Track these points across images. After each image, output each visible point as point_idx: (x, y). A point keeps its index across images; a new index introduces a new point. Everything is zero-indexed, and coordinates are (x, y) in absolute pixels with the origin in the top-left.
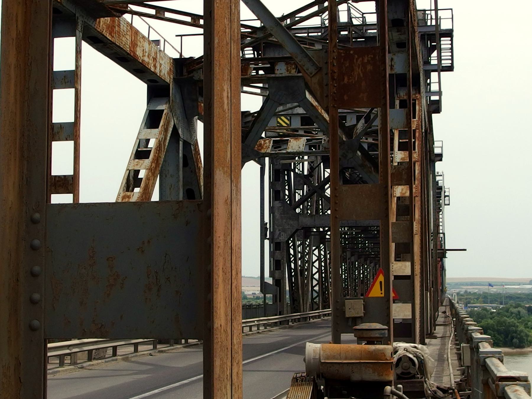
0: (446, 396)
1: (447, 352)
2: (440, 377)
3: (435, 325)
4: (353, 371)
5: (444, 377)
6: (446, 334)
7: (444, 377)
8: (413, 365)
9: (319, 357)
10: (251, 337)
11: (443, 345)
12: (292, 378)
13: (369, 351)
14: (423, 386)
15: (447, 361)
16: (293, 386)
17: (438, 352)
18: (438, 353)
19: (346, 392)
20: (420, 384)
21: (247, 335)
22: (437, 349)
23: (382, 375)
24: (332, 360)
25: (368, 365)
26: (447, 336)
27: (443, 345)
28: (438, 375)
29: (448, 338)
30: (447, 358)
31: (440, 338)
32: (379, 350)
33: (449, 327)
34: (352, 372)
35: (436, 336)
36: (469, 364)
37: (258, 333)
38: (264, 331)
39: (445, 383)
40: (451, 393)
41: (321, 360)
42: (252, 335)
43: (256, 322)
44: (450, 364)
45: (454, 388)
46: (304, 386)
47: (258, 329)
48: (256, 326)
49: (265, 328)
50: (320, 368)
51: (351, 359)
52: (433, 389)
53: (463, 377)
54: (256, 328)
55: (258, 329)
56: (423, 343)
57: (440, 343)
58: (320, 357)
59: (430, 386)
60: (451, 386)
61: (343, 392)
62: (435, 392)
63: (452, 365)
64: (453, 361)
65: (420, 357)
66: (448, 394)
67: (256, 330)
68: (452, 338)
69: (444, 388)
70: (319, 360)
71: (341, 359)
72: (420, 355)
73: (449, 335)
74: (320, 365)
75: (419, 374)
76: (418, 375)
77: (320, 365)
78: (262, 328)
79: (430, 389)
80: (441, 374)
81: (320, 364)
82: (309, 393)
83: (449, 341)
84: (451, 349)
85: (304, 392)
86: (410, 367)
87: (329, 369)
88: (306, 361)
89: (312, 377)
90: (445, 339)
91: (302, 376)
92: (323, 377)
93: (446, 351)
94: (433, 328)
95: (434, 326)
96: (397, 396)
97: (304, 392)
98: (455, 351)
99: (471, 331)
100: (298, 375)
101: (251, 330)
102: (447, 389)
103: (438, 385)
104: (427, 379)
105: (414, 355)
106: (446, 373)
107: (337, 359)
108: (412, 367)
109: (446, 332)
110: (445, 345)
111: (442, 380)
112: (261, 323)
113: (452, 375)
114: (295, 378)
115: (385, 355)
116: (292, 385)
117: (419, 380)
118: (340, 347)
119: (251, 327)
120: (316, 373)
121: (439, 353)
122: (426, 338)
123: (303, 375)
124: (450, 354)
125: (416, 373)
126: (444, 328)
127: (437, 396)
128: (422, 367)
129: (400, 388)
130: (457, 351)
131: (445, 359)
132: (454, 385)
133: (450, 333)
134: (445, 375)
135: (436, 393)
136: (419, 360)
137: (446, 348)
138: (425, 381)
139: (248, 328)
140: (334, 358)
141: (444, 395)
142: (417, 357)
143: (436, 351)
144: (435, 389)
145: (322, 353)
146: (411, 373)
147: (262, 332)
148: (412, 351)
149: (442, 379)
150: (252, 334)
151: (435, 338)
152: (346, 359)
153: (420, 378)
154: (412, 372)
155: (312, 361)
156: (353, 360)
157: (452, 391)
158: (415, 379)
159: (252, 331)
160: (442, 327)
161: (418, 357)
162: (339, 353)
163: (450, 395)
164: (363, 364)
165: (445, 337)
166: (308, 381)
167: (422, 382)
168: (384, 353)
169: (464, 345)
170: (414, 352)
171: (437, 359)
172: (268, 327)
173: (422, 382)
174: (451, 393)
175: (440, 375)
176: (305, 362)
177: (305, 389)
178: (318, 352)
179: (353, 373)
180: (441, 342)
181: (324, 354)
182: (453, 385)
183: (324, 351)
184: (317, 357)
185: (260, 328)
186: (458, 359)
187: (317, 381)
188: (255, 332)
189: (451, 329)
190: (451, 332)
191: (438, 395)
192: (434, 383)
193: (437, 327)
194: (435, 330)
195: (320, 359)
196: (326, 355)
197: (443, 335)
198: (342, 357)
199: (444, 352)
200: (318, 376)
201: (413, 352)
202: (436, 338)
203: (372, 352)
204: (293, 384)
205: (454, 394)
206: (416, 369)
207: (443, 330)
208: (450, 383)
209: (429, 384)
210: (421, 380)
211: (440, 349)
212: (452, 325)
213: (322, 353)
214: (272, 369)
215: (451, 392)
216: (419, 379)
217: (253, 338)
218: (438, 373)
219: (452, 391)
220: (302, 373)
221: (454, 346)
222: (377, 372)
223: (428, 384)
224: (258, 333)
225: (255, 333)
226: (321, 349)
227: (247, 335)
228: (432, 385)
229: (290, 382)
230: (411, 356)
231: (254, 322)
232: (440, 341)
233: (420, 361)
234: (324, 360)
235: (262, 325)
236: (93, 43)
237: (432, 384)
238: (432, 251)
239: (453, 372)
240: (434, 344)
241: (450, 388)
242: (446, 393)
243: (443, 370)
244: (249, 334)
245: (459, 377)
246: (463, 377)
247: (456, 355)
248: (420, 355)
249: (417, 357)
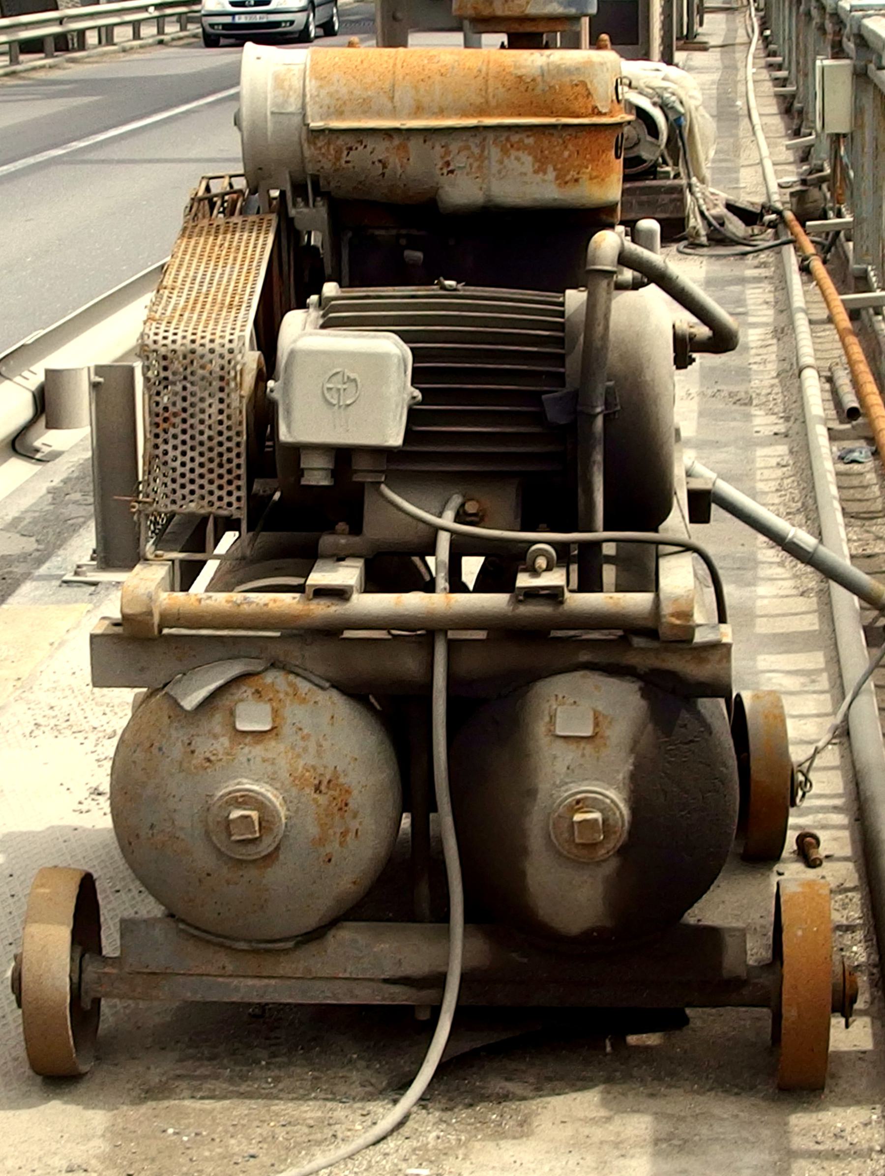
0: (756, 232)
1: (744, 89)
2: (729, 170)
3: (702, 10)
4: (448, 164)
5: (742, 170)
6: (735, 38)
7: (742, 170)
8: (650, 134)
9: (299, 105)
10: (135, 56)
11: (730, 68)
12: (187, 201)
13: (520, 77)
14: (682, 201)
15: (747, 120)
16: (190, 237)
17: (715, 91)
18: (715, 95)
19: (419, 255)
20: (674, 196)
21: (124, 50)
22: (713, 83)
23: (577, 180)
24: (359, 120)
25: (515, 138)
26: (738, 41)
27: (730, 68)
28: (724, 165)
29: (742, 47)
30: (745, 108)
31: (719, 49)
32: (561, 71)
33: (743, 15)
34: (445, 171)
35: (706, 43)
36: (843, 129)
37: (161, 42)
38: (180, 38)
39: (748, 190)
40: (772, 225)
41: (309, 121)
42: (142, 51)
43: (151, 9)
44: (758, 128)
45: (779, 206)
46: (237, 235)
47: (161, 31)
48: (155, 20)
49: (183, 29)
50: (307, 153)
51: (441, 112)
52: (714, 212)
53: (805, 167)
54: (154, 30)
55: (161, 31)
56: (668, 59)
57: (719, 64)
58: (304, 107)
59: (705, 203)
60: (769, 200)
61: (408, 253)
62: (721, 222)
63: (763, 129)
64: (767, 120)
65: (672, 108)
66: (763, 225)
67: (153, 36)
68: (756, 49)
69: (751, 208)
70: (300, 118)
71: (394, 113)
72: (673, 98)
73: (745, 39)
74: (306, 146)
75: (670, 162)
76: (667, 165)
77: (306, 146)
78: (172, 29)
79: (707, 213)
80: (733, 161)
81: (304, 136)
82: (255, 264)
83: (747, 57)
84: (755, 82)
85: (235, 259)
86: (639, 140)
87: (344, 158)
88: (244, 124)
89: (275, 193)
90: (734, 52)
91: (232, 190)
92: (317, 192)
93: (741, 88)
94: (697, 19)
95: (698, 13)
96: (635, 269)
97: (235, 259)
98: (768, 87)
99: (860, 13)
100: (217, 187)
101: (136, 36)
102: (757, 209)
103: (731, 197)
104: (694, 180)
105: (656, 99)
106: (748, 156)
107: (379, 114)
108: (649, 138)
109: (736, 31)
110: (736, 68)
111: (737, 180)
112: (169, 11)
113: (768, 164)
114: (201, 200)
115: (589, 94)
116: (185, 229)
117: (669, 182)
118: (391, 62)
119: (136, 25)
120: (288, 176)
121: (719, 94)
122: (679, 49)
123: (236, 187)
124: (756, 96)
125: (660, 160)
126: (727, 20)
127: (729, 235)
128: (679, 140)
129: (650, 233)
130: (775, 86)
131: (741, 113)
132: (778, 199)
133: (748, 35)
134: (746, 163)
135: (722, 224)
136: (672, 117)
137: (739, 78)
138: (690, 186)
139: (129, 30)
140: (366, 107)
141: (749, 230)
142: (664, 107)
143: (709, 89)
144: (721, 210)
145: (311, 86)
146: (645, 161)
147: (173, 39)
148: (648, 87)
149: (734, 175)
150: (141, 47)
151: (703, 47)
152: (418, 110)
153: (672, 175)
154: (645, 155)
155: (270, 125)
156: (449, 117)
157: (773, 217)
158: (655, 179)
159: (142, 39)
160: (721, 17)
161: (667, 105)
162: (387, 86)
163: (770, 230)
164: (491, 136)
165: (733, 45)
166: (258, 212)
167: (679, 190)
168: (584, 84)
169: (827, 62)
170: (653, 89)
171: (715, 113)
172: (190, 26)
173: (679, 190)
174: (772, 225)
175: (729, 165)
176: (240, 129)
177: (242, 249)
178: (297, 84)
179: (452, 172)
180: (722, 59)
181: (323, 93)
182: (775, 197)
183: (322, 78)
184: (293, 106)
185: (168, 29)
186: (780, 113)
187: (292, 212)
188: (150, 41)
189: (748, 22)
190: (750, 30)
191: (727, 230)
192: (717, 192)
193: (707, 17)
194: (701, 24)
195: (304, 116)
196: (330, 95)
197: (725, 39)
198: (398, 104)
199: (736, 93)
200: (299, 189)
201: (651, 91)
202: (705, 49)
203: (534, 80)
204: (191, 224)
205: (780, 227)
206: (659, 146)
207: (724, 26)
208: (765, 192)
209: (703, 194)
210: (677, 182)
211: (721, 83)
212: (753, 9)
213: (311, 86)
214: (192, 154)
215: (771, 222)
216: (668, 178)
217: (142, 60)
218: (722, 156)
219: (773, 217)
220: (231, 177)
221: (765, 71)
222: (555, 169)
223: (699, 195)
224: (161, 42)
225: (151, 45)
226: (308, 73)
227: (124, 50)
228: (712, 197)
229: (178, 219)
230: (645, 104)
231: (147, 10)
232: (718, 56)
233: (675, 120)
234: (322, 119)
235: (174, 18)
236: (774, 544)
237: (713, 194)
238: (239, 418)
239: (770, 153)
240: (702, 68)
241: (767, 208)
242: (755, 224)
243: (736, 149)
244: (132, 48)
245: (792, 168)
246: (805, 167)
247: (774, 101)
248: (673, 98)
249: (664, 107)
